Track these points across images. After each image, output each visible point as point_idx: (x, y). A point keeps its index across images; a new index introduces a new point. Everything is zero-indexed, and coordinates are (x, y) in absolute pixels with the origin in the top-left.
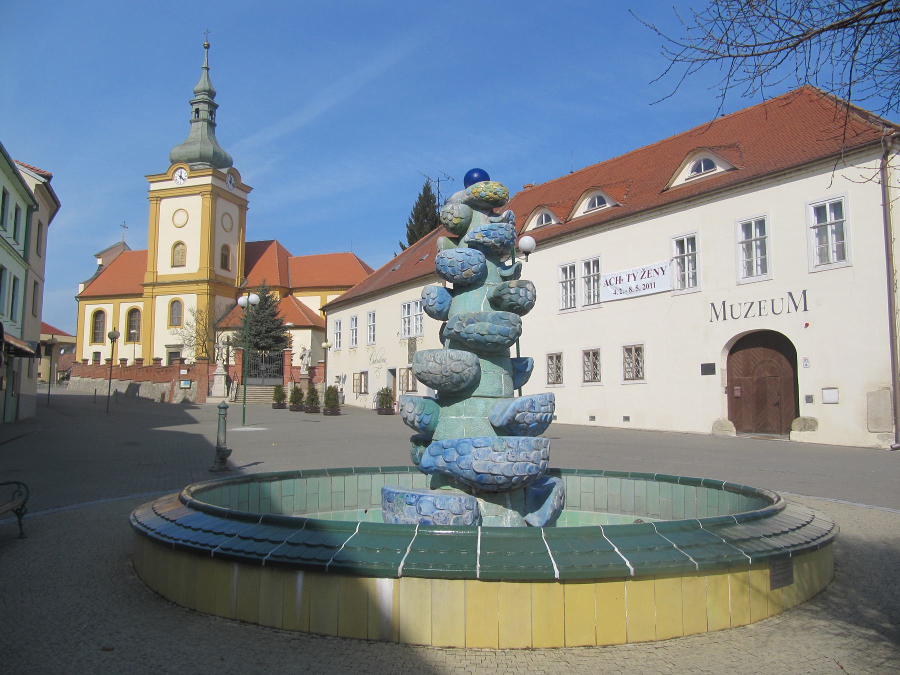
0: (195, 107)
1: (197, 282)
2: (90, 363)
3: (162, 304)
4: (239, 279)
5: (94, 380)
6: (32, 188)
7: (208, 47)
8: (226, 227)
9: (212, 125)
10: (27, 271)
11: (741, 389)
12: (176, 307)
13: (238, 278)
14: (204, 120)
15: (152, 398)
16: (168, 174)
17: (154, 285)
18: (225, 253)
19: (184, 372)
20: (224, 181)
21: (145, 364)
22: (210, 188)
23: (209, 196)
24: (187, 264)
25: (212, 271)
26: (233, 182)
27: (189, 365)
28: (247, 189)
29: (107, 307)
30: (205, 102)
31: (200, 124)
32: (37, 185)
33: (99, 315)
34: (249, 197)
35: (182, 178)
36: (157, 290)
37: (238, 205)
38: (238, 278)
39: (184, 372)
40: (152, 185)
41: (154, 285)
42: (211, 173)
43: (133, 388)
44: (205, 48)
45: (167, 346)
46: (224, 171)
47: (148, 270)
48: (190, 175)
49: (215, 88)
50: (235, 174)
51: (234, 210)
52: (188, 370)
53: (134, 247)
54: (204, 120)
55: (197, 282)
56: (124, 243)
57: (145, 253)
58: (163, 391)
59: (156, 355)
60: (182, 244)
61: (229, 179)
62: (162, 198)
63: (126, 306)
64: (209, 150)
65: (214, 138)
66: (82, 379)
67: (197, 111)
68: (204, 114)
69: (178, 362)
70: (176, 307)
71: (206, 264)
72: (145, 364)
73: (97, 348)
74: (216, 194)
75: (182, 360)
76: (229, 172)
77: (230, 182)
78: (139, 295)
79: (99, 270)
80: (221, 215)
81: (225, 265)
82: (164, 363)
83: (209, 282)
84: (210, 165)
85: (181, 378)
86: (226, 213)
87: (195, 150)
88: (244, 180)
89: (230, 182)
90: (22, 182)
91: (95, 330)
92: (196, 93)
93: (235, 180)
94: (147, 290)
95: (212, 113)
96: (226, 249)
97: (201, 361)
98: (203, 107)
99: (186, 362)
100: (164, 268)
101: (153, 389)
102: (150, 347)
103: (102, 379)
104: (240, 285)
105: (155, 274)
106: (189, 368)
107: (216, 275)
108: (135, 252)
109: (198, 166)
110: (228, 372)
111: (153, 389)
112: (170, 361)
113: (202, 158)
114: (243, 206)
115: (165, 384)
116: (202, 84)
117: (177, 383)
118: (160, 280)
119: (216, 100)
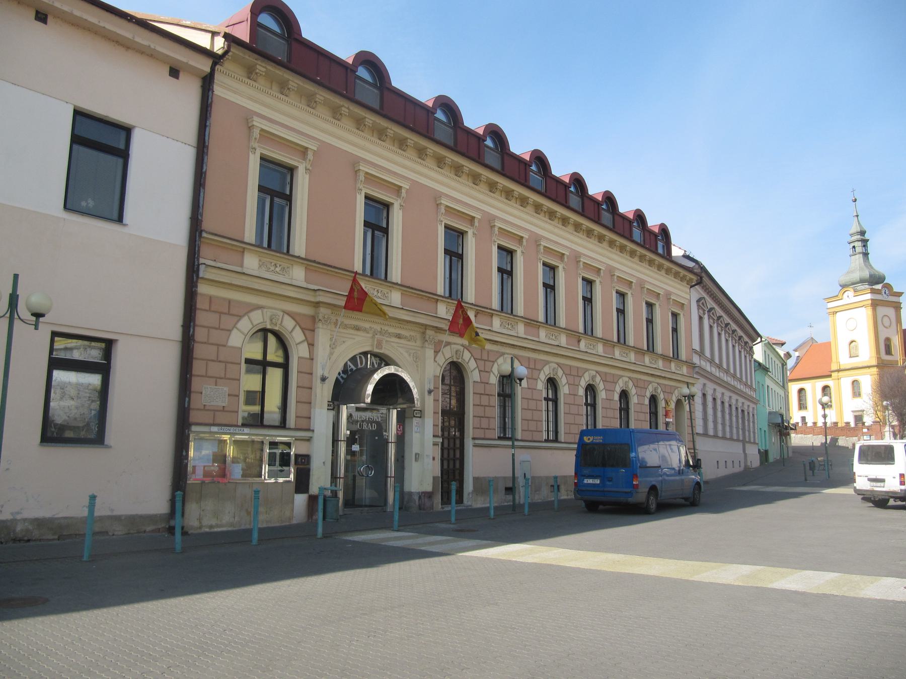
0: (852, 245)
1: (869, 367)
2: (800, 425)
3: (846, 383)
4: (901, 360)
5: (805, 436)
6: (782, 356)
7: (855, 201)
8: (885, 325)
9: (866, 255)
10: (785, 393)
11: (442, 443)
12: (855, 384)
13: (900, 359)
14: (860, 253)
15: (847, 446)
16: (839, 296)
17: (838, 371)
18: (888, 343)
19: (865, 430)
20: (880, 293)
21: (839, 425)
22: (870, 302)
23: (870, 307)
24: (860, 355)
25: (879, 358)
26: (887, 292)
27: (868, 426)
28: (899, 294)
29: (806, 385)
30: (858, 241)
31: (857, 256)
32: (784, 354)
33: (801, 391)
34: (901, 299)
35: (849, 297)
36: (841, 374)
37: (894, 307)
38: (900, 359)
39: (865, 430)
40: (828, 304)
41: (838, 371)
42: (870, 291)
43: (834, 440)
44: (854, 202)
45: (853, 411)
46: (879, 287)
47: (833, 361)
48: (856, 295)
49: (865, 228)
50: (888, 287)
51: (891, 312)
52: (868, 429)
53: (820, 340)
54: (860, 253)
55: (869, 367)
56: (812, 338)
57: (829, 344)
58: (853, 442)
59: (846, 421)
60: (855, 341)
61: (883, 292)
62: (836, 312)
63: (821, 383)
64: (866, 274)
65: (869, 262)
66: (797, 435)
67: (854, 247)
68: (859, 249)
69: (861, 424)
70: (855, 384)
71: (874, 354)
72: (839, 425)
73: (803, 413)
74: (875, 304)
75: (863, 423)
76: (883, 287)
77: (885, 293)
78: (830, 376)
79: (797, 360)
80: (881, 318)
81: (888, 351)
82: (852, 425)
83: (877, 366)
84: (868, 285)
85: (863, 434)
86: (885, 316)
87: (856, 276)
88: (896, 289)
89: (885, 293)
90: (777, 352)
91: (800, 401)
92: (851, 235)
93: (889, 290)
94: (834, 374)
95: (865, 246)
96: (888, 341)
97: (875, 423)
98: (858, 245)
99: (866, 424)
100: (842, 358)
101: (847, 441)
102: (840, 412)
103: (811, 435)
104: (903, 364)
105: (838, 363)
106: (868, 428)
107: (883, 360)
108: (821, 344)
109: (860, 287)
110: (894, 430)
111: (847, 441)
112: (856, 424)
113: (862, 281)
114: (897, 307)
115: (854, 438)
116: (855, 228)
117: (862, 437)
118: (842, 367)
119: (867, 236)
